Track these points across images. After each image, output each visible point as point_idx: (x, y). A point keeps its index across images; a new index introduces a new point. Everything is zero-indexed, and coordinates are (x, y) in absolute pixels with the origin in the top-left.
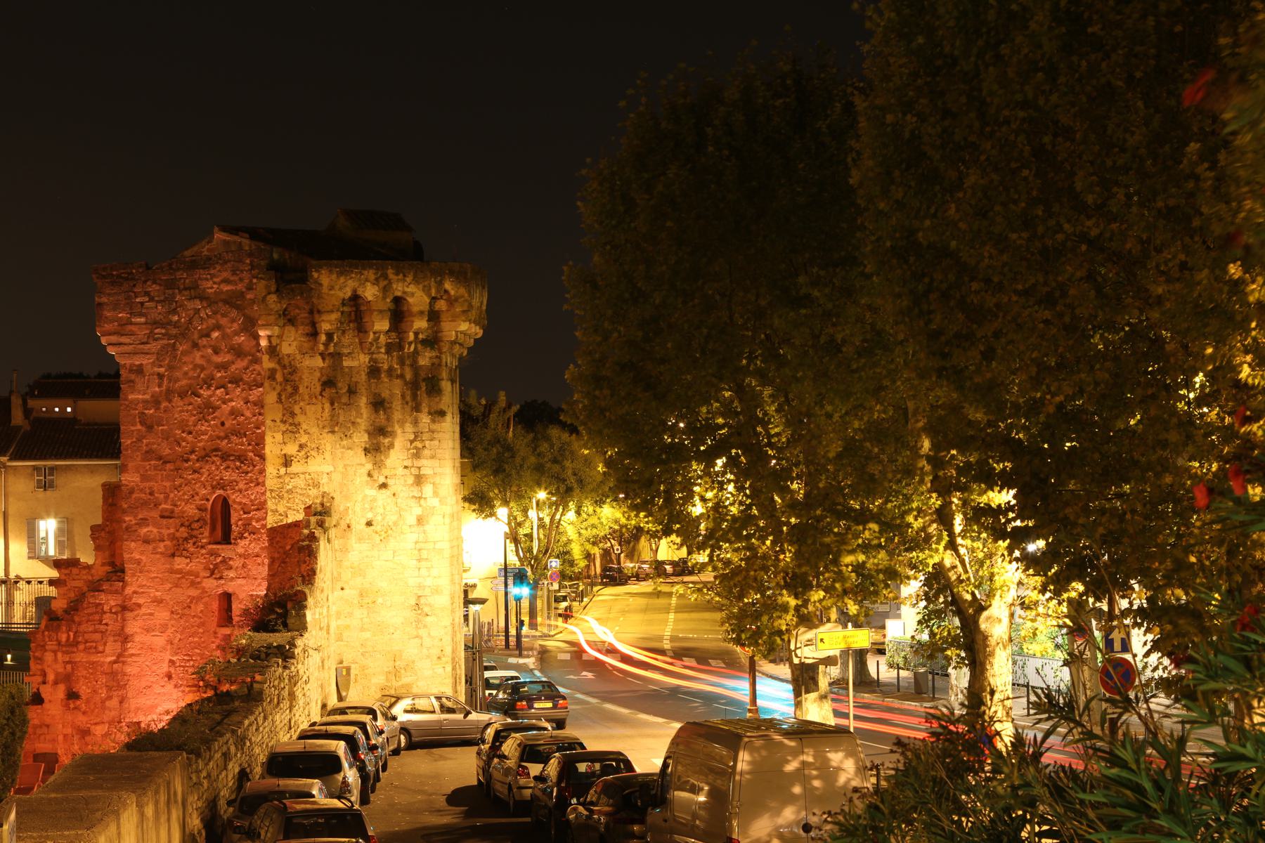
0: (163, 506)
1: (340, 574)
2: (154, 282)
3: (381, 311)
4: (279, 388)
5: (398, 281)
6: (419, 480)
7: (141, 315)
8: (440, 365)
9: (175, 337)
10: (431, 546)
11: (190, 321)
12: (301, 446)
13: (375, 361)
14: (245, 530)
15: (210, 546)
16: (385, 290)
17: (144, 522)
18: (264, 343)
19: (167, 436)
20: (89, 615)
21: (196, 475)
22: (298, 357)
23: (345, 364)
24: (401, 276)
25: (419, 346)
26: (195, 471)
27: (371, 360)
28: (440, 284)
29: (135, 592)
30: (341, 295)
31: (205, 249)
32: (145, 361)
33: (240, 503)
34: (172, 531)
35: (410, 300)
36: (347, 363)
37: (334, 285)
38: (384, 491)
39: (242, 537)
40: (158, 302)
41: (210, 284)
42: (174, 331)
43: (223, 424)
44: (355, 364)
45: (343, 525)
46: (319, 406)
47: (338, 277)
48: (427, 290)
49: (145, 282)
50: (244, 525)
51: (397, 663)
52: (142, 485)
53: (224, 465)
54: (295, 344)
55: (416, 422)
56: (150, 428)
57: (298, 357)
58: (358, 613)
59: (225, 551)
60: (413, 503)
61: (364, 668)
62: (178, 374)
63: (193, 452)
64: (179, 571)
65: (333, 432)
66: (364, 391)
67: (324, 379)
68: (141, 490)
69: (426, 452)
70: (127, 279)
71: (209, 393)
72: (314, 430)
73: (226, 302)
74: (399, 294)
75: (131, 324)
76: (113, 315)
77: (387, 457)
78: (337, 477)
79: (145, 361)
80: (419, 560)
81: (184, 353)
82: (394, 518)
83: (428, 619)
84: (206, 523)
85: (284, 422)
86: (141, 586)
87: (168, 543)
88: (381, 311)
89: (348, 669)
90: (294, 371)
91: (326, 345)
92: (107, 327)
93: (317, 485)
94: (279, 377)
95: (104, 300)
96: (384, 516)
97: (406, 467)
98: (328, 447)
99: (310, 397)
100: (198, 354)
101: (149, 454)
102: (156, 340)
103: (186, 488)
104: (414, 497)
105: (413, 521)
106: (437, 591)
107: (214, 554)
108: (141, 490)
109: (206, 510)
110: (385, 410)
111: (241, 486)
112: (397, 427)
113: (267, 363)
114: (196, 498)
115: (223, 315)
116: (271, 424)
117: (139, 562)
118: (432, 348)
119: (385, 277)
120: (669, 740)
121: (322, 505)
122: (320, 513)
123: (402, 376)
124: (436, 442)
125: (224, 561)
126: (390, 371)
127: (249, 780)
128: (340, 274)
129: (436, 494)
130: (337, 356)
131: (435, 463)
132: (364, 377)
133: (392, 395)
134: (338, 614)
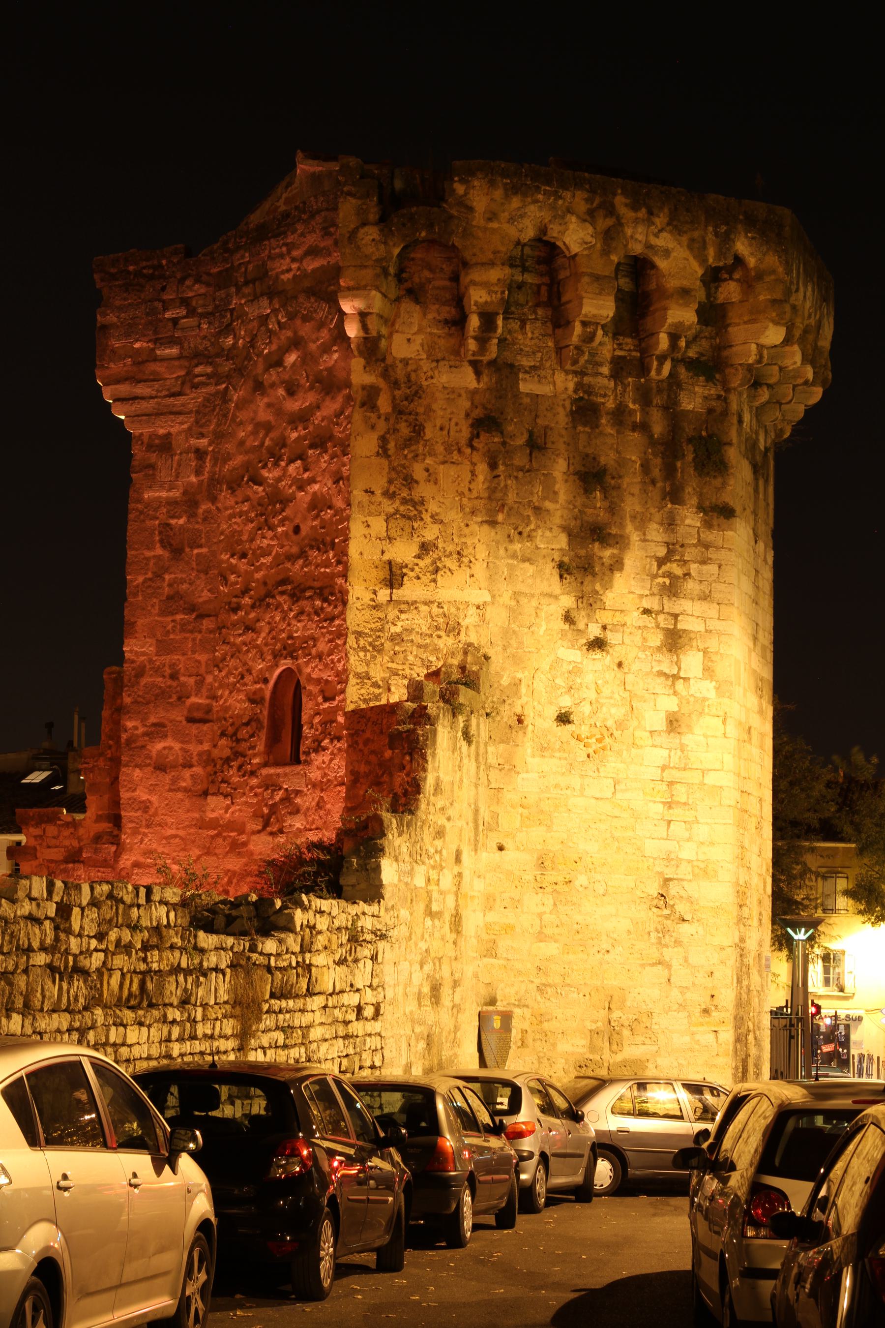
0: (194, 700)
1: (495, 816)
2: (198, 280)
3: (597, 278)
4: (382, 426)
5: (636, 221)
6: (674, 640)
7: (172, 341)
8: (725, 413)
9: (228, 377)
10: (694, 777)
11: (252, 343)
12: (425, 548)
13: (589, 390)
14: (325, 733)
15: (265, 771)
16: (609, 237)
17: (158, 730)
18: (352, 330)
19: (205, 567)
21: (250, 635)
23: (523, 387)
24: (642, 213)
25: (683, 372)
26: (248, 628)
27: (579, 386)
28: (725, 240)
29: (137, 865)
30: (512, 231)
31: (281, 200)
32: (175, 427)
33: (319, 681)
34: (206, 746)
35: (662, 264)
36: (526, 386)
37: (501, 215)
38: (597, 655)
39: (318, 748)
40: (202, 316)
41: (285, 263)
42: (227, 367)
43: (297, 530)
44: (545, 389)
45: (507, 715)
46: (467, 466)
47: (507, 196)
48: (697, 248)
49: (182, 281)
50: (324, 723)
51: (615, 1015)
52: (159, 660)
53: (296, 608)
54: (419, 339)
55: (670, 524)
56: (177, 552)
57: (426, 366)
58: (533, 902)
59: (291, 778)
60: (659, 685)
61: (540, 1018)
62: (229, 446)
63: (245, 591)
64: (213, 824)
65: (492, 523)
66: (562, 447)
67: (478, 413)
68: (157, 671)
69: (691, 586)
70: (151, 278)
71: (277, 473)
72: (453, 516)
73: (311, 292)
74: (637, 249)
75: (156, 359)
76: (123, 345)
77: (608, 586)
78: (497, 616)
79: (175, 427)
80: (669, 805)
81: (242, 405)
82: (618, 712)
83: (685, 928)
84: (260, 728)
85: (389, 495)
86: (148, 853)
87: (198, 770)
88: (597, 278)
89: (507, 1018)
90: (417, 393)
91: (483, 341)
92: (115, 368)
93: (454, 629)
94: (384, 404)
95: (112, 318)
96: (596, 706)
97: (646, 612)
98: (482, 553)
99: (448, 450)
100: (262, 402)
101: (175, 601)
102: (195, 386)
103: (232, 663)
104: (661, 674)
105: (658, 722)
106: (705, 871)
107: (271, 785)
108: (157, 671)
109: (261, 701)
110: (605, 491)
111: (322, 646)
112: (629, 528)
113: (360, 375)
114: (248, 679)
115: (306, 319)
116: (365, 498)
117: (145, 807)
118: (710, 379)
119: (610, 210)
121: (463, 668)
122: (458, 684)
123: (644, 427)
124: (713, 568)
125: (287, 799)
126: (619, 415)
128: (514, 190)
129: (708, 671)
130: (504, 371)
131: (711, 610)
132: (562, 418)
133: (622, 463)
134: (490, 901)
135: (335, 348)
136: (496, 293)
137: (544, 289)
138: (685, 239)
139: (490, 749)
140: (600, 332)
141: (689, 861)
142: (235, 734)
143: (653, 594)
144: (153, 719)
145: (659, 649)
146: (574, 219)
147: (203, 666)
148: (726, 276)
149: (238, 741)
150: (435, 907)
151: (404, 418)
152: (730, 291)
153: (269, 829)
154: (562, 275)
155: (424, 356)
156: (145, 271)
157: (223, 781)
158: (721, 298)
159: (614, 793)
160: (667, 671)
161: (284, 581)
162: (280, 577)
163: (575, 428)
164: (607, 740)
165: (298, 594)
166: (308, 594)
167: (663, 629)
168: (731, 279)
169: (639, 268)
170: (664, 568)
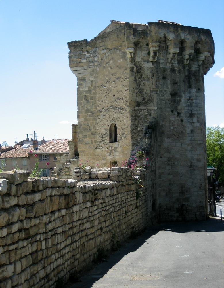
1: (160, 151)
4: (135, 75)
7: (84, 58)
17: (85, 136)
20: (65, 172)
22: (143, 63)
27: (172, 66)
42: (96, 64)
51: (183, 189)
59: (115, 145)
74: (182, 38)
80: (192, 148)
90: (141, 68)
91: (154, 57)
104: (189, 122)
120: (106, 276)
127: (186, 76)
135: (121, 59)
136: (157, 48)
137: (164, 47)
138: (192, 36)
139: (158, 138)
140: (176, 55)
141: (196, 159)
142: (102, 137)
143: (187, 106)
144: (84, 134)
145: (188, 117)
146: (171, 33)
147: (94, 123)
148: (198, 43)
149: (103, 138)
150: (153, 170)
151: (139, 73)
152: (199, 46)
153: (111, 155)
154: (168, 44)
155: (142, 61)
156: (78, 45)
157: (100, 146)
158: (198, 48)
159: (182, 145)
160: (190, 121)
161: (111, 106)
162: (110, 105)
163: (171, 74)
164: (180, 136)
165: (115, 108)
166: (117, 108)
167: (189, 113)
168: (199, 44)
169: (182, 42)
170: (189, 101)
